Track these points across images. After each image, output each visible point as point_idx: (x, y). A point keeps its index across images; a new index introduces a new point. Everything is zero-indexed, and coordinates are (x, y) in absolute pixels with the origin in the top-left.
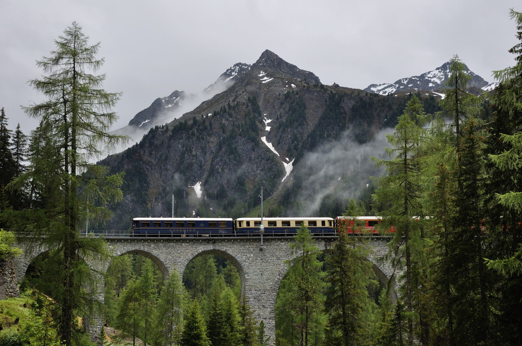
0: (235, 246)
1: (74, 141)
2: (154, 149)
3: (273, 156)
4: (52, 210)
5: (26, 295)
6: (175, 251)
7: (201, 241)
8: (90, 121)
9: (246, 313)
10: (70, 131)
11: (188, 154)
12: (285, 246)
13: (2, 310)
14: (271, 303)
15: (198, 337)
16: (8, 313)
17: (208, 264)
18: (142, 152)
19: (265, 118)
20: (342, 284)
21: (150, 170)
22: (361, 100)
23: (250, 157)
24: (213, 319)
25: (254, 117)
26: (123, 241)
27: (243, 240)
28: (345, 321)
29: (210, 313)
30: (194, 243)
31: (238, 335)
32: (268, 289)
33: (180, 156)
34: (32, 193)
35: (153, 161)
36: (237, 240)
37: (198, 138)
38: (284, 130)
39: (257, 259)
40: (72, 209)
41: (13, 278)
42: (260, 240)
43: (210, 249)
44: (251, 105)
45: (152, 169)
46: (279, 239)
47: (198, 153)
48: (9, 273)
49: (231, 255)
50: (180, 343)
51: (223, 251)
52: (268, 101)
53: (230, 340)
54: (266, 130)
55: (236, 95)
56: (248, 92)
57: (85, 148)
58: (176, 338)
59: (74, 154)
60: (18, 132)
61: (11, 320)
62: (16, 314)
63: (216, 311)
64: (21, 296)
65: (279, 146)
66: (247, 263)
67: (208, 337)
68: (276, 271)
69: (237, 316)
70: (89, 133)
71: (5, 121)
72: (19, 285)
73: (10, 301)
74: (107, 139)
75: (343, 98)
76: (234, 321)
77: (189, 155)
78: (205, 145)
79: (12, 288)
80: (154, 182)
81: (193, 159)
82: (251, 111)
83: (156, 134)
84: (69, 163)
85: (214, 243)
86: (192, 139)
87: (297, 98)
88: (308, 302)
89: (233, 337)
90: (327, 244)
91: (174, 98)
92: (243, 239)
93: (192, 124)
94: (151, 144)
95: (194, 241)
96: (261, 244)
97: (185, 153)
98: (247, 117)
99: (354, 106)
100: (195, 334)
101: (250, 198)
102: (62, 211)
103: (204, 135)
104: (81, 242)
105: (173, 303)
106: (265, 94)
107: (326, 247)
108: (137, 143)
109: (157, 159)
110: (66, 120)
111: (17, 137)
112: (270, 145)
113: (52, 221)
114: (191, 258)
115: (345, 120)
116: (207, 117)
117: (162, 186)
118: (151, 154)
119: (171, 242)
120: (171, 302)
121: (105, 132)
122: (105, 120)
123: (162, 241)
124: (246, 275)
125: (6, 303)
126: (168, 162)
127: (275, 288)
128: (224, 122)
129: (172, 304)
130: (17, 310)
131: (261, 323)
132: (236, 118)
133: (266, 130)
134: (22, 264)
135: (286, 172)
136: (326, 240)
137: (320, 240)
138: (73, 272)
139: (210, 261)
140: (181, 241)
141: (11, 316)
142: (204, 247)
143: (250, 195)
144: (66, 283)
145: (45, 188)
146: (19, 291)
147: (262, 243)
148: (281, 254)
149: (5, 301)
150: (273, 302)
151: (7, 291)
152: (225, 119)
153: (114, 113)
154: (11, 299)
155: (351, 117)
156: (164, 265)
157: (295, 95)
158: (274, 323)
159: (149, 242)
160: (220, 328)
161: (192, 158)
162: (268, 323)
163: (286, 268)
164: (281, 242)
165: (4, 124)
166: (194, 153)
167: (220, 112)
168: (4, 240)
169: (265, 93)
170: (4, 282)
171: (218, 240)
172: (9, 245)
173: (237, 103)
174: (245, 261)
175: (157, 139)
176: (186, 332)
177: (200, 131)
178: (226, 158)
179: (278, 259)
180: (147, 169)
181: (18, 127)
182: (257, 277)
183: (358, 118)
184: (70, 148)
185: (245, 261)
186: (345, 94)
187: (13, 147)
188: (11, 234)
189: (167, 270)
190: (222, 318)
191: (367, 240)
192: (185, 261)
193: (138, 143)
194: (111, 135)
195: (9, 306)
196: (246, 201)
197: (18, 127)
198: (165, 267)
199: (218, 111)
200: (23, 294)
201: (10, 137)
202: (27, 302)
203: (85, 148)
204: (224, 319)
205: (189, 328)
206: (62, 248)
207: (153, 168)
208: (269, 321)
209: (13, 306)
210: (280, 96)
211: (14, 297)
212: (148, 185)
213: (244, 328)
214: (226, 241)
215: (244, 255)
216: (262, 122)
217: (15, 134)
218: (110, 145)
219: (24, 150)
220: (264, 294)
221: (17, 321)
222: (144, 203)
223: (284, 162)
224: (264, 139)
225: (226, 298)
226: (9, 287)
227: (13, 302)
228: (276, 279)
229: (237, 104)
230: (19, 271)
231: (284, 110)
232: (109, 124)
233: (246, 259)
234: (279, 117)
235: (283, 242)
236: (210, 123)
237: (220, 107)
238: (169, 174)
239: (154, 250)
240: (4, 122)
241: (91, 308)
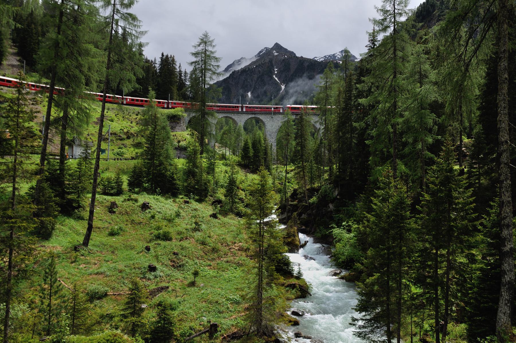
1: (205, 75)
10: (203, 71)
15: (248, 148)
22: (311, 62)
59: (205, 80)
73: (183, 132)
74: (216, 75)
112: (276, 79)
122: (216, 68)
179: (278, 121)
184: (203, 78)
224: (274, 76)
241: (211, 136)
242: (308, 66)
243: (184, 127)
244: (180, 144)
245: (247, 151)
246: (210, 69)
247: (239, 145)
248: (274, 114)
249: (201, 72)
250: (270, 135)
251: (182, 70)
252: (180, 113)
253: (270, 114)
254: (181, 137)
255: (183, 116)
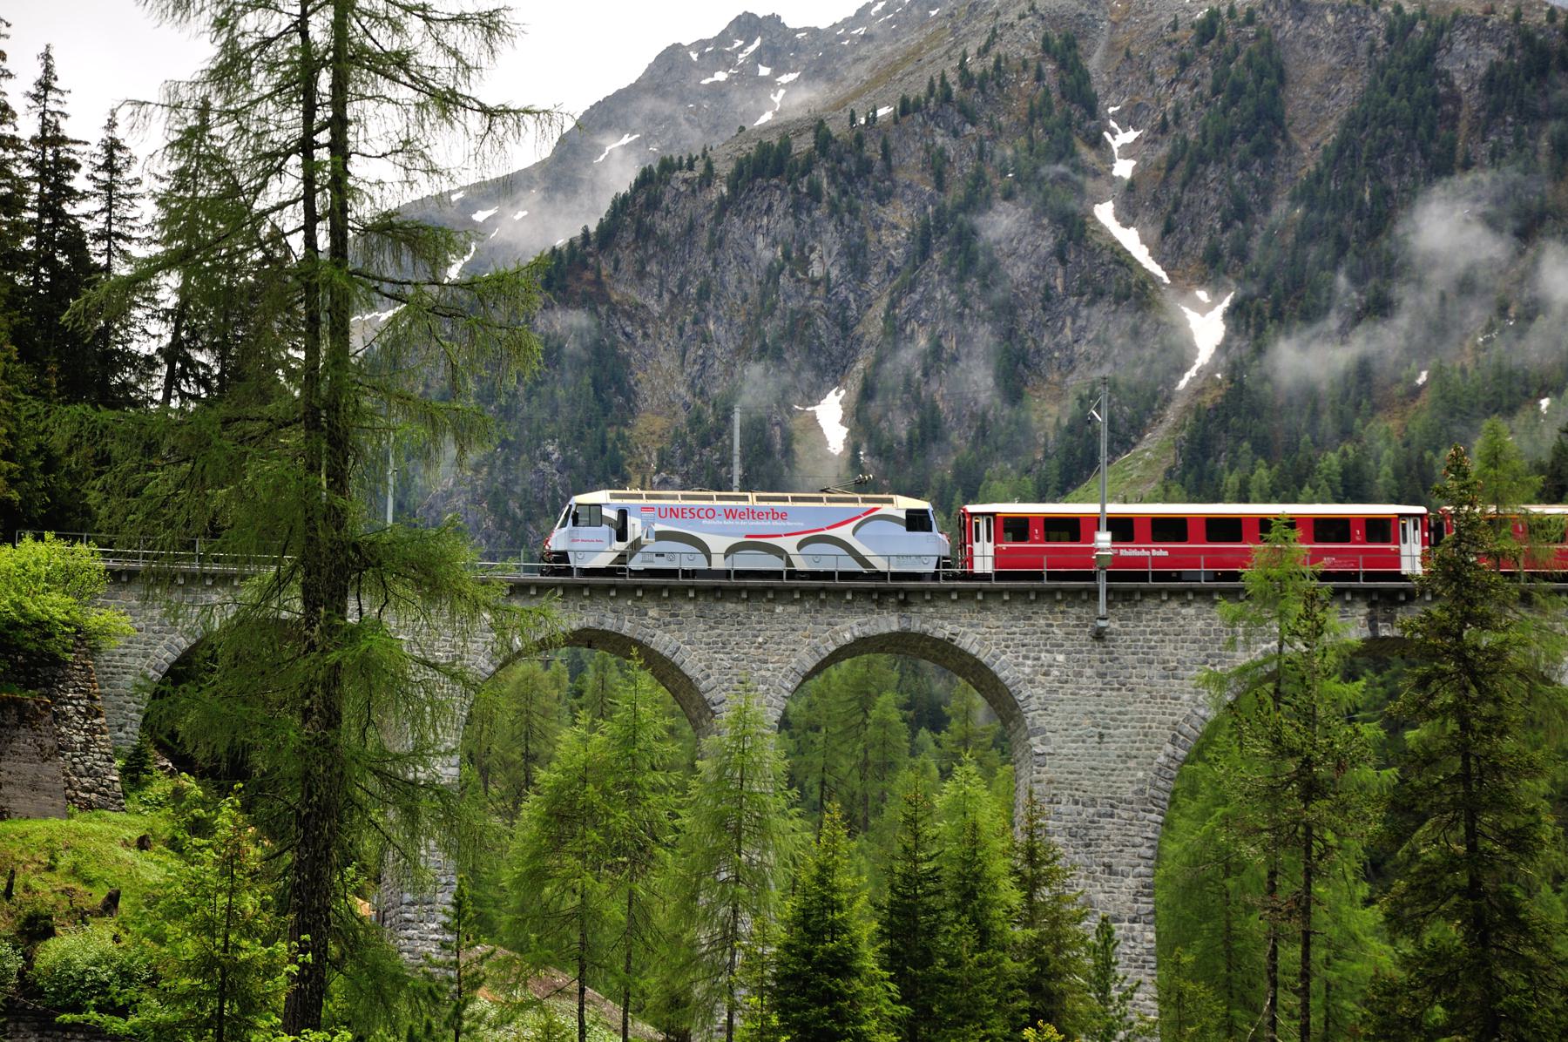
0: (992, 621)
1: (339, 124)
2: (654, 255)
3: (1144, 284)
4: (253, 410)
5: (146, 803)
6: (744, 636)
7: (849, 597)
8: (408, 45)
9: (1040, 876)
10: (324, 81)
11: (792, 274)
12: (1194, 618)
13: (52, 857)
14: (1140, 857)
15: (843, 965)
16: (74, 871)
17: (874, 713)
18: (606, 270)
19: (1113, 124)
20: (1465, 726)
21: (639, 341)
22: (1528, 39)
23: (1048, 287)
24: (904, 896)
25: (1067, 122)
26: (533, 592)
27: (1025, 593)
28: (1475, 882)
29: (891, 871)
30: (823, 602)
31: (1009, 965)
32: (1129, 796)
33: (760, 283)
34: (167, 397)
35: (651, 302)
36: (1000, 592)
37: (834, 209)
38: (1192, 173)
39: (1079, 674)
40: (333, 407)
41: (95, 732)
42: (1094, 594)
43: (886, 631)
44: (1054, 72)
45: (646, 335)
46: (1173, 593)
47: (834, 273)
48: (78, 712)
49: (972, 657)
50: (769, 988)
51: (941, 640)
52: (1128, 54)
53: (976, 982)
54: (1116, 173)
55: (994, 30)
56: (1043, 18)
57: (384, 155)
58: (752, 969)
59: (339, 181)
60: (112, 146)
61: (87, 898)
62: (109, 875)
63: (916, 862)
64: (129, 805)
65: (1169, 241)
66: (1040, 691)
67: (882, 967)
68: (1160, 723)
69: (1001, 887)
70: (405, 94)
71: (58, 101)
72: (119, 763)
73: (81, 823)
74: (475, 121)
75: (1446, 35)
76: (992, 905)
77: (798, 281)
78: (862, 236)
79: (91, 772)
80: (653, 389)
81: (811, 297)
82: (1055, 96)
83: (663, 193)
84: (320, 219)
85: (904, 604)
86: (809, 211)
87: (1247, 40)
88: (1312, 806)
89: (988, 971)
90: (1380, 613)
91: (739, 43)
92: (1025, 592)
93: (810, 152)
94: (644, 233)
95: (823, 596)
96: (1096, 611)
97: (782, 269)
98: (1037, 121)
99: (1494, 67)
100: (832, 953)
101: (1047, 457)
102: (290, 418)
103: (859, 196)
104: (372, 543)
105: (739, 825)
106: (1115, 24)
107: (1374, 628)
108: (586, 230)
109: (666, 297)
110: (305, 35)
111: (109, 166)
112: (1131, 240)
113: (253, 458)
114: (810, 664)
115: (1454, 127)
116: (872, 120)
117: (687, 406)
118: (641, 274)
119: (727, 600)
120: (732, 824)
121: (466, 92)
122: (468, 42)
123: (691, 594)
124: (1034, 740)
125: (69, 831)
126: (710, 306)
127: (1155, 793)
128: (939, 140)
129: (737, 833)
130: (111, 860)
131: (1101, 926)
132: (990, 124)
133: (1116, 173)
134: (130, 678)
135: (1197, 350)
136: (1375, 598)
137: (1348, 597)
138: (338, 665)
139: (882, 699)
140: (770, 596)
141: (89, 882)
142: (862, 619)
143: (1046, 445)
144: (310, 710)
145: (220, 377)
146: (118, 786)
147: (1102, 609)
148: (1181, 654)
149: (64, 823)
150: (1150, 853)
151: (70, 786)
152: (946, 129)
153: (509, 9)
154: (86, 815)
155: (1482, 114)
156: (700, 694)
157: (1239, 25)
158: (1151, 936)
159: (640, 599)
160: (931, 932)
161: (807, 293)
162: (1126, 939)
163: (1201, 712)
164: (1183, 605)
165: (53, 114)
166: (817, 270)
167: (927, 101)
168: (59, 577)
169: (1114, 18)
170: (60, 748)
171: (922, 592)
172: (80, 597)
173: (998, 61)
174: (1031, 681)
175: (668, 212)
176: (794, 947)
177: (841, 179)
178: (946, 290)
179: (1170, 673)
180: (626, 334)
181: (112, 125)
182: (1081, 749)
183: (1510, 119)
184: (322, 155)
185: (1031, 681)
186: (1455, 17)
187: (94, 205)
188: (85, 555)
189: (714, 713)
190: (938, 892)
191: (1554, 598)
192: (785, 676)
193: (593, 229)
194: (491, 103)
195: (78, 841)
196: (1028, 471)
197: (112, 125)
198: (705, 702)
199: (918, 98)
200: (134, 796)
201: (77, 167)
202: (151, 830)
203: (384, 155)
204: (950, 896)
205: (807, 929)
206: (294, 569)
207: (650, 331)
208: (1132, 929)
209: (94, 844)
210: (1175, 29)
211: (101, 807)
212: (628, 400)
213: (1032, 933)
214: (954, 597)
215: (1026, 657)
216: (1097, 143)
217: (99, 151)
218: (487, 146)
219: (134, 219)
220: (1112, 816)
221: (112, 901)
222: (615, 473)
223: (1186, 310)
224: (1105, 213)
225: (960, 808)
226: (80, 767)
227: (96, 827)
228: (1162, 759)
229: (997, 67)
230: (121, 708)
231: (1191, 89)
232: (484, 59)
233: (1036, 673)
234: (1169, 118)
235: (1188, 603)
236: (885, 147)
237: (926, 81)
238: (714, 356)
239: (659, 632)
240: (52, 106)
241: (411, 815)
242: (1493, 81)
243: (94, 759)
244: (50, 953)
245: (829, 997)
246: (401, 60)
247: (729, 937)
248: (1126, 597)
249: (300, 84)
250: (1083, 836)
251: (68, 129)
252: (55, 605)
253: (1073, 596)
254: (58, 881)
255: (86, 640)
